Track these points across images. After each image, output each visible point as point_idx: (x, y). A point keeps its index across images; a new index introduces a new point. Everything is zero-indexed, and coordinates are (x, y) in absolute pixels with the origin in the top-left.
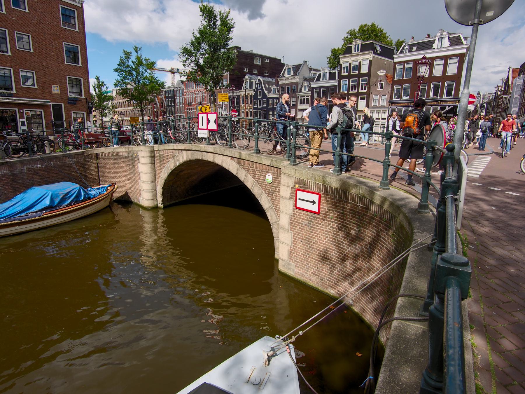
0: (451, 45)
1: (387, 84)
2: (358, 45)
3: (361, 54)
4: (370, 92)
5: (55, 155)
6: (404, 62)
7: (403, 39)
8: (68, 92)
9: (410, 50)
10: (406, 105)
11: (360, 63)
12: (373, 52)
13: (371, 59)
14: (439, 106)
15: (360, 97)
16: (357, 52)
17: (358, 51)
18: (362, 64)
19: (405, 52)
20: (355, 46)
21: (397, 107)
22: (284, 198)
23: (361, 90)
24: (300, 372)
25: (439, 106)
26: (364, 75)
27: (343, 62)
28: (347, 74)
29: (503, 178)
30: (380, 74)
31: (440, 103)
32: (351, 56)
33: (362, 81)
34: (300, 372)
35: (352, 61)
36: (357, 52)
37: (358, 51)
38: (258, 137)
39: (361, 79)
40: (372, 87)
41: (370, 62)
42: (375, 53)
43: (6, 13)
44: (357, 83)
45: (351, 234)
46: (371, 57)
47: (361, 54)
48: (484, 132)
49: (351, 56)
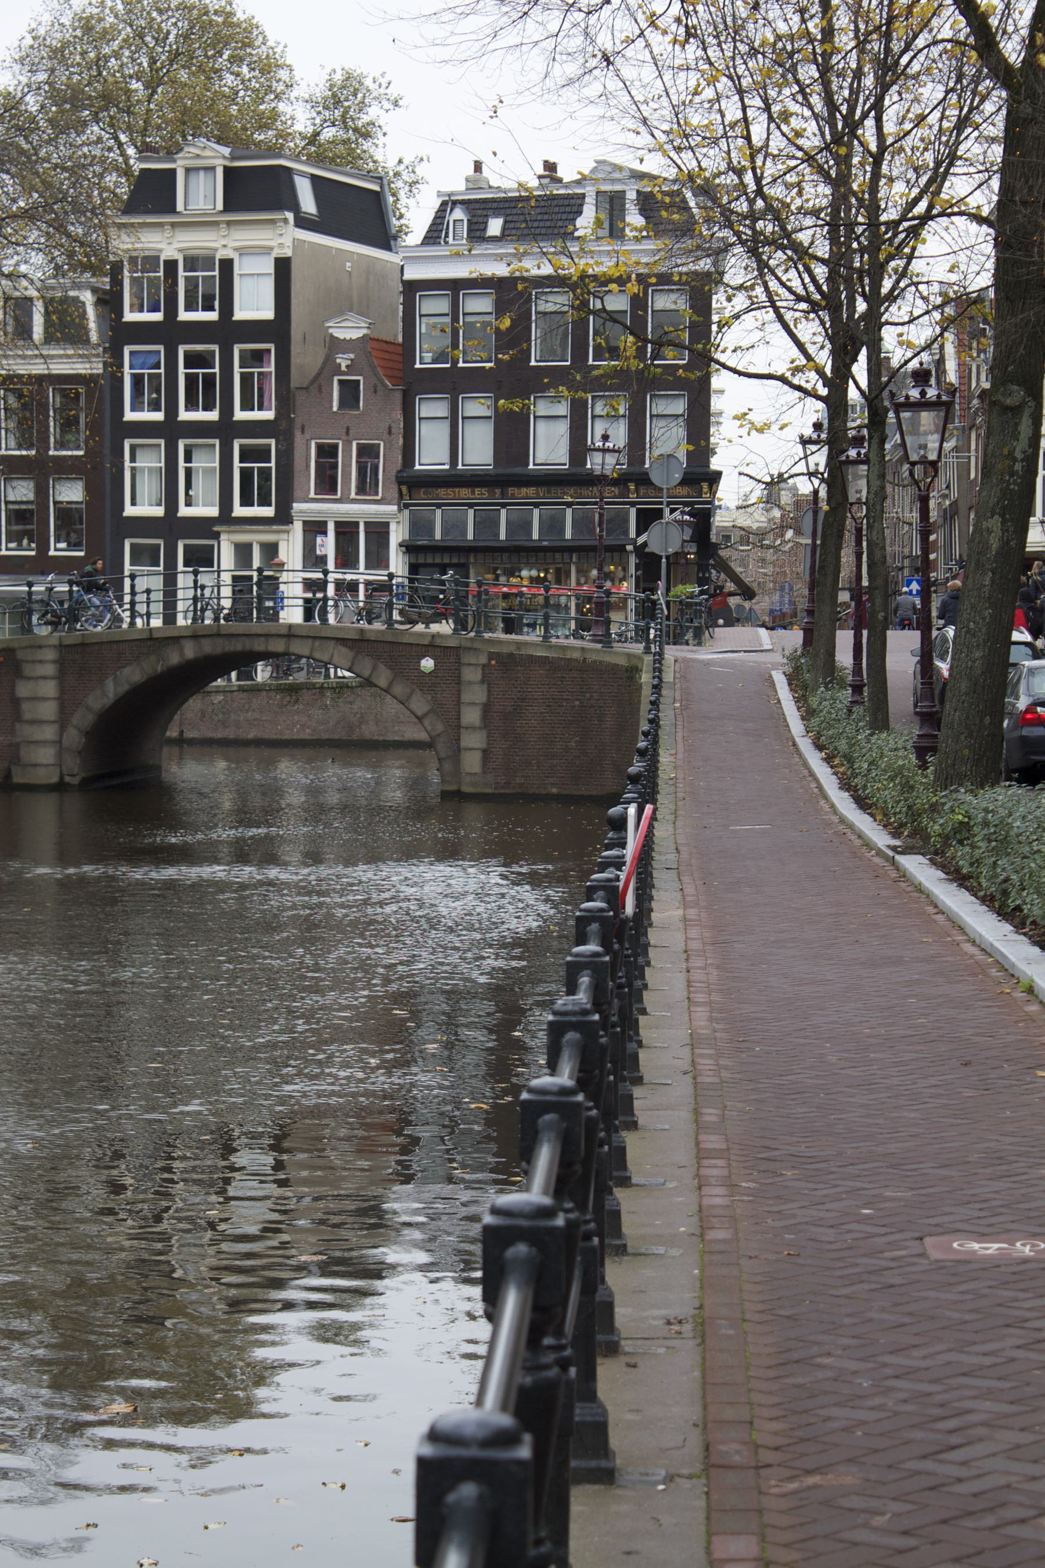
0: (231, 204)
1: (379, 387)
3: (229, 223)
4: (291, 421)
6: (454, 287)
9: (477, 233)
10: (480, 494)
11: (227, 266)
12: (290, 216)
13: (288, 252)
14: (633, 504)
15: (242, 448)
18: (236, 271)
19: (450, 239)
21: (439, 506)
22: (470, 683)
23: (243, 409)
25: (633, 504)
26: (254, 330)
27: (236, 249)
28: (158, 317)
30: (340, 334)
31: (637, 490)
32: (173, 225)
33: (192, 360)
35: (236, 249)
39: (181, 350)
40: (301, 398)
41: (283, 268)
42: (303, 222)
46: (288, 241)
47: (229, 223)
48: (240, 1359)
49: (173, 225)
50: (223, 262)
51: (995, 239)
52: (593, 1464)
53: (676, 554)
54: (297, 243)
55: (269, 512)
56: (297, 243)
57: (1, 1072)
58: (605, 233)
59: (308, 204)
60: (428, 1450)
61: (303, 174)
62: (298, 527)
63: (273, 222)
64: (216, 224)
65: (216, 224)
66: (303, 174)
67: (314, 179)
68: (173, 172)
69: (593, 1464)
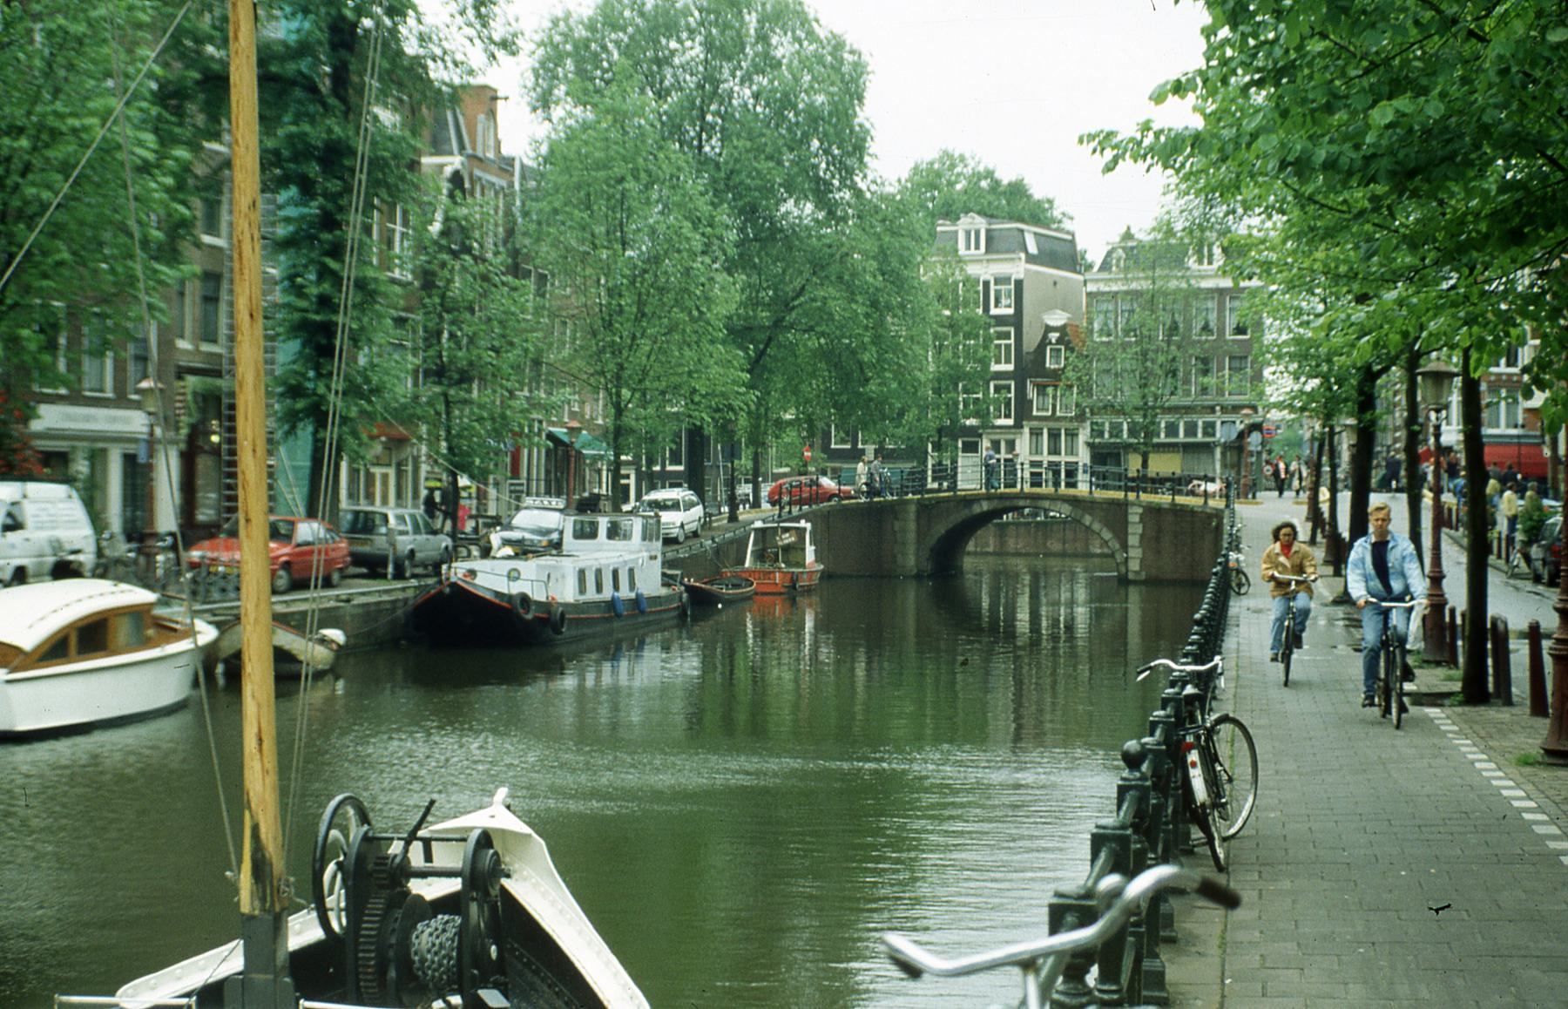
2: (977, 233)
3: (988, 261)
5: (1143, 623)
7: (1125, 229)
8: (537, 832)
12: (1023, 256)
13: (1021, 276)
16: (973, 251)
17: (977, 247)
20: (968, 233)
24: (232, 849)
29: (915, 942)
34: (232, 849)
36: (973, 251)
37: (977, 247)
38: (1218, 408)
41: (1019, 284)
42: (1031, 259)
43: (481, 992)
44: (1012, 341)
45: (356, 362)
46: (1022, 271)
47: (988, 261)
50: (1016, 281)
51: (611, 604)
52: (1157, 994)
53: (1455, 494)
54: (1027, 271)
55: (1010, 422)
56: (1027, 271)
57: (1, 834)
58: (225, 401)
59: (1032, 248)
60: (1055, 901)
61: (1029, 232)
62: (1026, 430)
63: (1013, 259)
64: (981, 261)
65: (981, 261)
66: (1029, 232)
67: (1035, 234)
68: (956, 232)
69: (1157, 994)
